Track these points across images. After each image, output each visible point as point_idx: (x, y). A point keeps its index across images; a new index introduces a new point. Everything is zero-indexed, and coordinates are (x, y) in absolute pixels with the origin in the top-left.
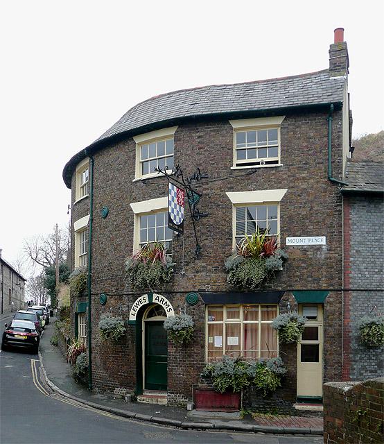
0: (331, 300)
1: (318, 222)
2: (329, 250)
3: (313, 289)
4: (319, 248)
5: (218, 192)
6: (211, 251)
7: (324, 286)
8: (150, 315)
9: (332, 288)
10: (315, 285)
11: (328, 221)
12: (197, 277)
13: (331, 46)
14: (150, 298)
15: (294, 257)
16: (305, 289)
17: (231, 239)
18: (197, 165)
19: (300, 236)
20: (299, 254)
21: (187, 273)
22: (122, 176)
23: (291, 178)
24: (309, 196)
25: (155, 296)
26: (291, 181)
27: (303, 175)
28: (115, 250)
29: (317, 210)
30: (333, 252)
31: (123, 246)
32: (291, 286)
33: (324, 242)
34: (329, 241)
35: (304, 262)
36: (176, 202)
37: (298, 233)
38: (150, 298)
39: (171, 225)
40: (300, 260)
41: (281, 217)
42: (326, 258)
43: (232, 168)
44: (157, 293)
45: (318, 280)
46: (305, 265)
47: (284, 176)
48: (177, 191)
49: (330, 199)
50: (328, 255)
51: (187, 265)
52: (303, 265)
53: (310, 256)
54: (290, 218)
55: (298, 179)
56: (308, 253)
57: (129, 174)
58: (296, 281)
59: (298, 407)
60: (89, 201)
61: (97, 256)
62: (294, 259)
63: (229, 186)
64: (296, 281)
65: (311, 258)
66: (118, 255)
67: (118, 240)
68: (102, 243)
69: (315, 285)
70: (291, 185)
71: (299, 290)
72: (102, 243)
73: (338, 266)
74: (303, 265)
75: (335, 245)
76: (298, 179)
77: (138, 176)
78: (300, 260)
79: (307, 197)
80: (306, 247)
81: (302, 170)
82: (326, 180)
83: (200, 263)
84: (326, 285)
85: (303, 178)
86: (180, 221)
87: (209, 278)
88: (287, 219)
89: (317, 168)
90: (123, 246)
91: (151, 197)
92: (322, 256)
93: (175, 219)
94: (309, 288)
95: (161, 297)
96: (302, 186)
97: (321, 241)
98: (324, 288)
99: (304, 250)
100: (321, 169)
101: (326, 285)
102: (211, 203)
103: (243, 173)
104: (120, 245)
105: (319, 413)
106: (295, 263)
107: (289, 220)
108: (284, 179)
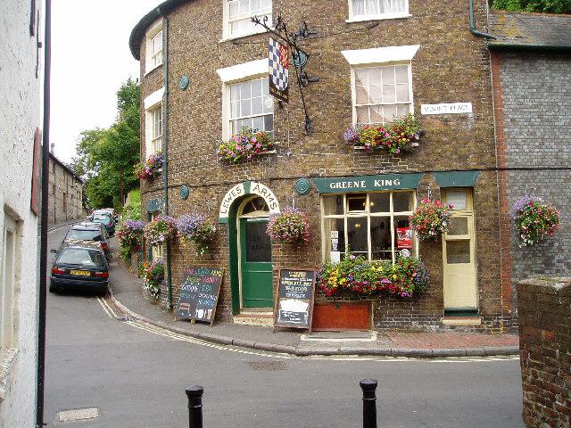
2: (478, 119)
4: (464, 118)
7: (473, 165)
9: (482, 167)
14: (247, 187)
19: (438, 103)
20: (437, 126)
25: (253, 185)
34: (476, 108)
35: (446, 134)
37: (437, 99)
38: (247, 187)
42: (474, 130)
44: (256, 181)
45: (463, 158)
49: (475, 53)
53: (453, 128)
56: (451, 123)
57: (216, 33)
58: (437, 160)
59: (447, 322)
73: (491, 141)
83: (311, 141)
85: (439, 31)
87: (323, 160)
91: (244, 60)
95: (262, 186)
96: (438, 42)
97: (466, 108)
99: (445, 120)
103: (361, 27)
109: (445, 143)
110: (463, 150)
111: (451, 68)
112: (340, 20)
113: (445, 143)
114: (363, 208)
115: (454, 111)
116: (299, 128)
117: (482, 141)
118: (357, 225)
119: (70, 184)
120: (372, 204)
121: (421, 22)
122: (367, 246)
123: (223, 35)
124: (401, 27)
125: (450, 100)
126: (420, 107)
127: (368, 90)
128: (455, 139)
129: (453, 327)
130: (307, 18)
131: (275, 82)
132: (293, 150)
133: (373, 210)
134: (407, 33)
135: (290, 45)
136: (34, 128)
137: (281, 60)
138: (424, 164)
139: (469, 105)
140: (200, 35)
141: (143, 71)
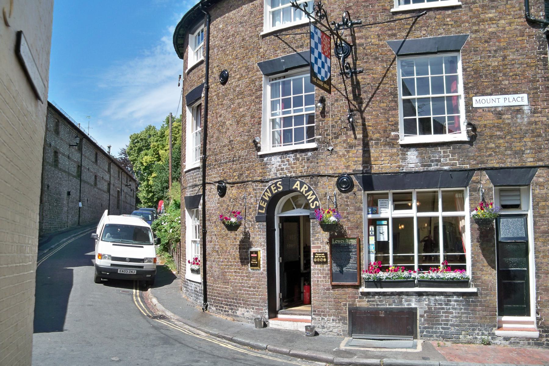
0: (541, 180)
1: (516, 75)
2: (534, 112)
3: (515, 165)
4: (518, 110)
5: (375, 41)
6: (370, 117)
7: (529, 161)
8: (287, 206)
9: (541, 163)
10: (517, 160)
11: (529, 73)
12: (350, 154)
13: (149, 128)
15: (486, 123)
16: (503, 165)
17: (396, 102)
18: (346, 8)
19: (491, 94)
20: (490, 119)
21: (337, 149)
22: (246, 30)
23: (474, 20)
24: (499, 42)
26: (474, 24)
27: (491, 15)
28: (238, 122)
29: (513, 60)
30: (539, 115)
31: (248, 119)
32: (482, 162)
33: (526, 102)
34: (533, 100)
35: (499, 128)
36: (320, 49)
37: (489, 91)
39: (315, 79)
40: (494, 126)
41: (464, 70)
42: (530, 123)
43: (392, 10)
46: (501, 134)
47: (464, 18)
48: (322, 37)
50: (533, 119)
51: (337, 138)
52: (498, 133)
53: (507, 121)
54: (476, 71)
55: (483, 21)
57: (256, 26)
58: (490, 155)
60: (204, 66)
61: (214, 133)
62: (485, 126)
63: (390, 32)
64: (490, 155)
65: (509, 124)
66: (241, 129)
67: (241, 110)
68: (220, 116)
69: (517, 160)
70: (475, 28)
71: (496, 169)
72: (220, 116)
74: (498, 133)
75: (541, 105)
76: (483, 21)
77: (268, 28)
78: (494, 126)
79: (497, 43)
80: (500, 109)
81: (489, 9)
82: (523, 20)
84: (532, 160)
85: (491, 19)
86: (326, 76)
88: (473, 73)
89: (508, 6)
90: (248, 119)
92: (523, 120)
93: (320, 72)
94: (508, 165)
96: (490, 30)
98: (529, 164)
99: (498, 113)
100: (514, 7)
101: (532, 160)
102: (366, 55)
103: (408, 16)
104: (243, 116)
105: (531, 341)
106: (487, 132)
107: (475, 73)
108: (463, 22)
109: (500, 137)
110: (517, 146)
111: (505, 58)
112: (385, 10)
113: (500, 137)
114: (410, 208)
115: (507, 104)
116: (342, 122)
117: (539, 136)
118: (403, 226)
119: (124, 182)
120: (418, 204)
121: (471, 10)
122: (388, 249)
123: (264, 28)
124: (449, 16)
125: (504, 92)
126: (471, 99)
127: (238, 330)
128: (509, 133)
129: (506, 339)
130: (350, 7)
131: (316, 70)
132: (336, 145)
133: (419, 209)
134: (456, 22)
135: (332, 33)
136: (44, 103)
137: (323, 48)
138: (475, 160)
139: (525, 96)
140: (241, 29)
141: (185, 67)
